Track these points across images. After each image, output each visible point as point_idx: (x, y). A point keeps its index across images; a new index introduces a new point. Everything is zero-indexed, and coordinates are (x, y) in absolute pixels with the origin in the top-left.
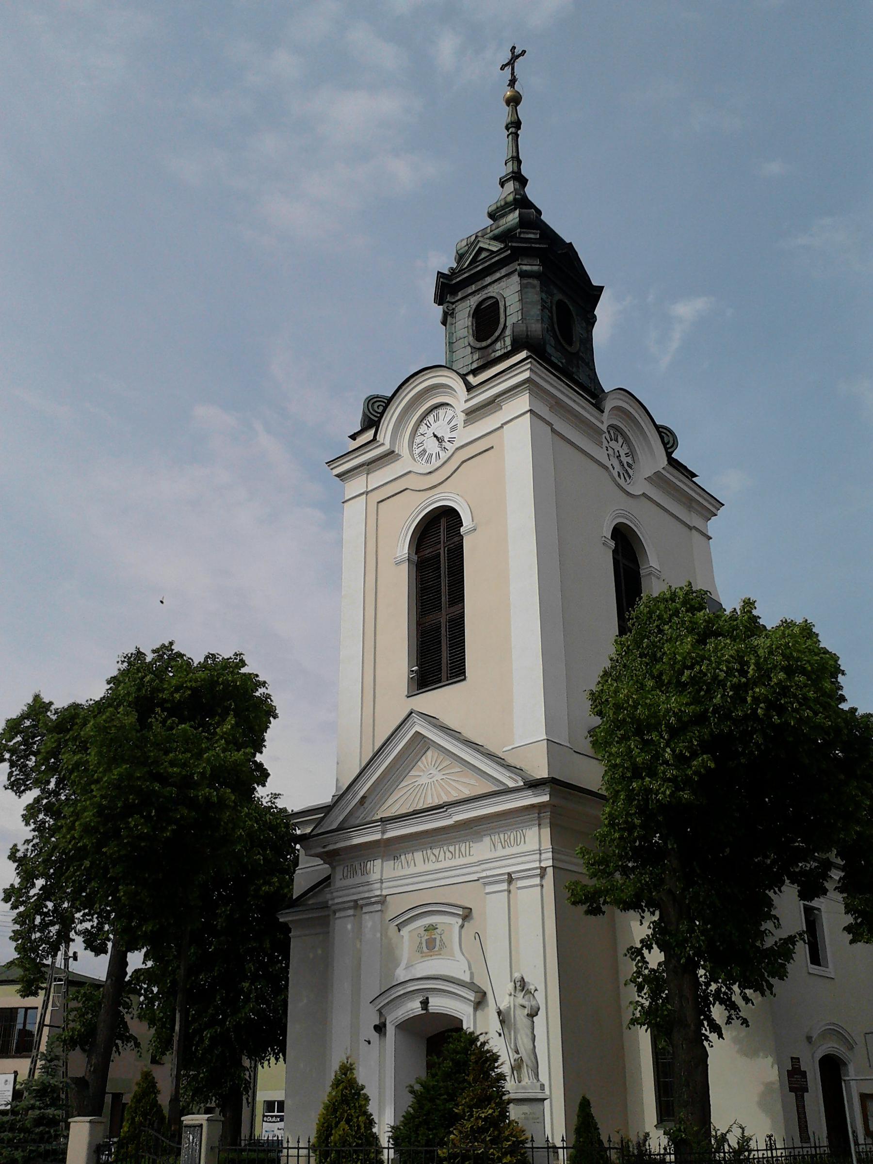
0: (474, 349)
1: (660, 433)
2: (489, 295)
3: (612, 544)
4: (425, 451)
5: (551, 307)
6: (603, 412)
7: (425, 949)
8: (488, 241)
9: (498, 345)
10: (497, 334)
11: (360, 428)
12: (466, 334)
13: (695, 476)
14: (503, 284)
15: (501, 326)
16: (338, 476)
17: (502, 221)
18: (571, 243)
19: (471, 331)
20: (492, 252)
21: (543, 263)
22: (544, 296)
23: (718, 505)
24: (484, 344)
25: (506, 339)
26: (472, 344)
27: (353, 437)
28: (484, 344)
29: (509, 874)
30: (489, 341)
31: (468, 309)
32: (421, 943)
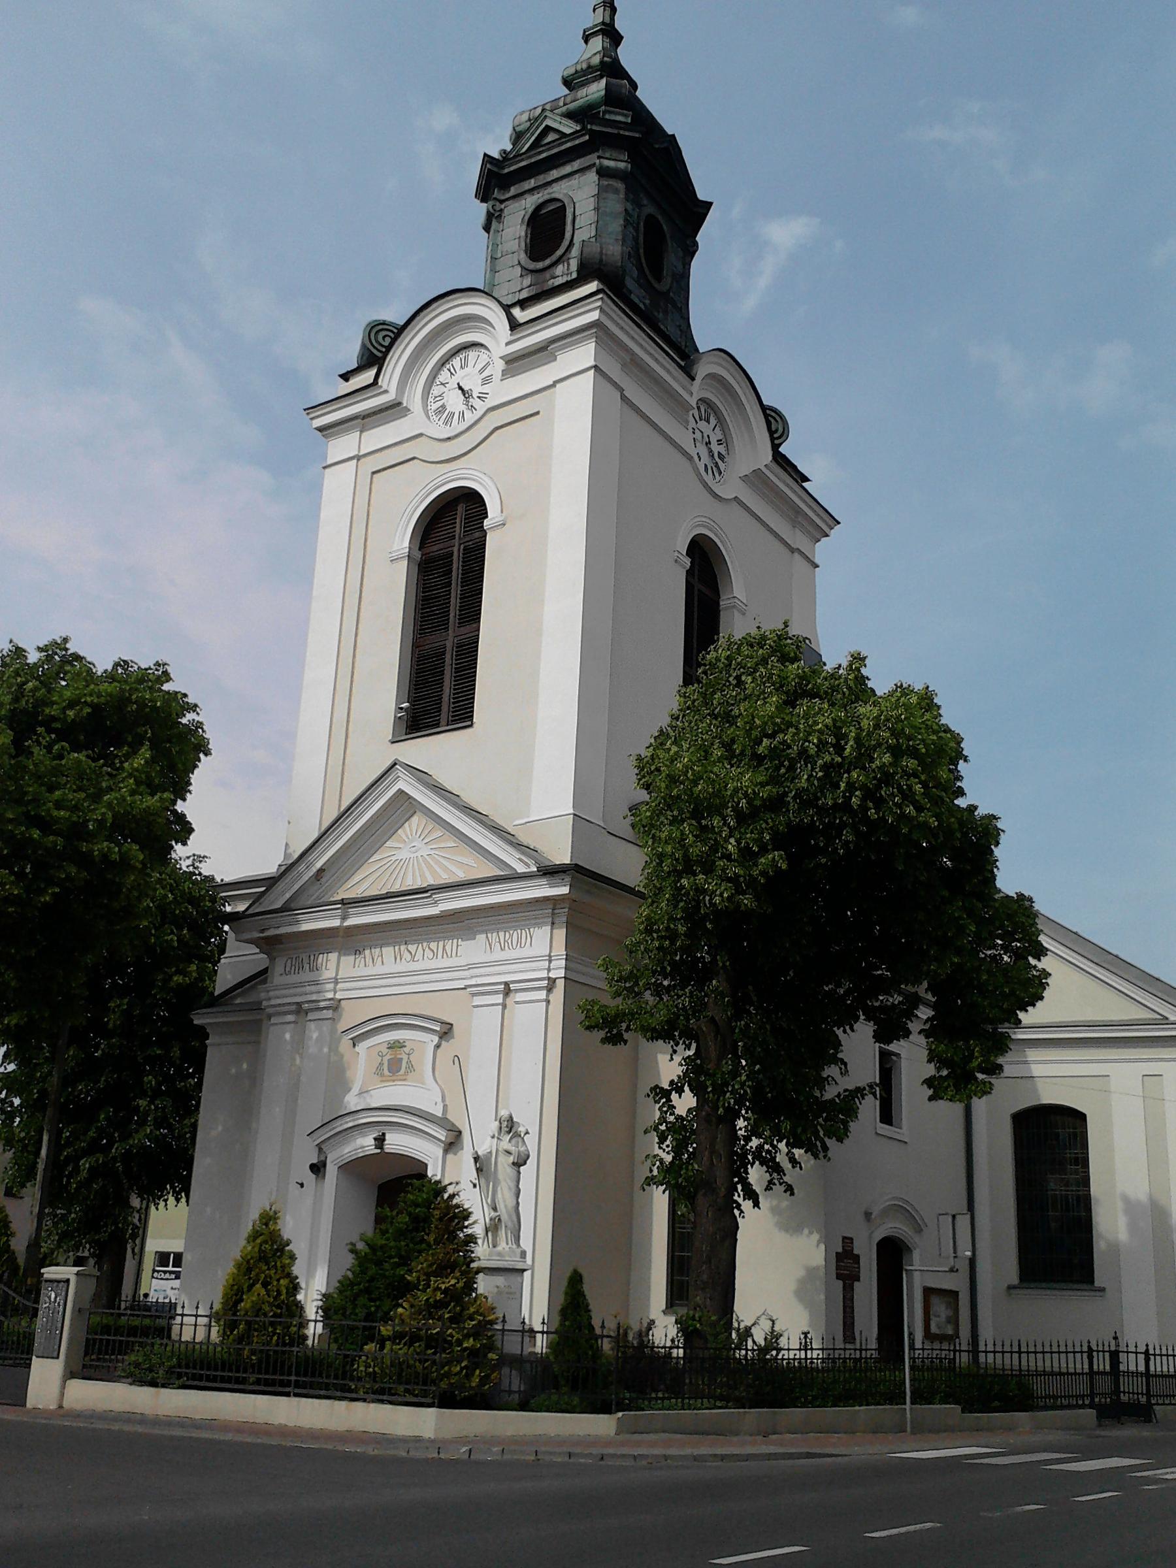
0: (526, 271)
1: (766, 416)
2: (553, 196)
3: (687, 562)
4: (443, 406)
5: (638, 223)
6: (693, 379)
7: (386, 1072)
8: (558, 118)
9: (560, 269)
10: (559, 253)
11: (356, 365)
12: (515, 248)
13: (807, 480)
14: (574, 182)
15: (566, 243)
16: (320, 429)
17: (582, 92)
18: (673, 136)
19: (523, 244)
20: (563, 135)
21: (632, 159)
22: (629, 207)
23: (831, 522)
24: (540, 265)
25: (571, 261)
26: (522, 263)
27: (346, 377)
28: (540, 265)
29: (507, 984)
30: (547, 262)
31: (523, 212)
32: (381, 1064)
